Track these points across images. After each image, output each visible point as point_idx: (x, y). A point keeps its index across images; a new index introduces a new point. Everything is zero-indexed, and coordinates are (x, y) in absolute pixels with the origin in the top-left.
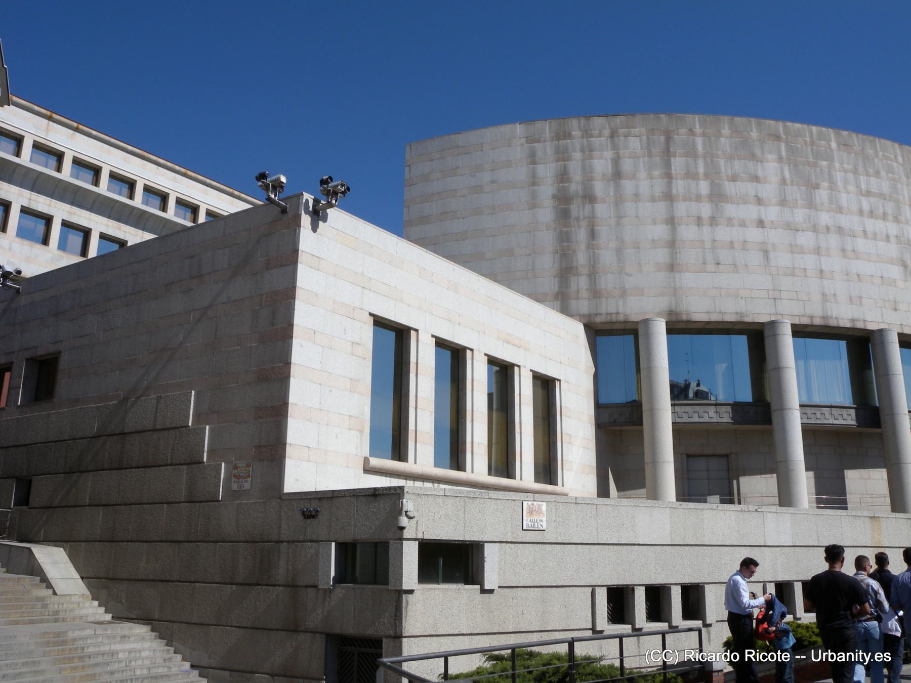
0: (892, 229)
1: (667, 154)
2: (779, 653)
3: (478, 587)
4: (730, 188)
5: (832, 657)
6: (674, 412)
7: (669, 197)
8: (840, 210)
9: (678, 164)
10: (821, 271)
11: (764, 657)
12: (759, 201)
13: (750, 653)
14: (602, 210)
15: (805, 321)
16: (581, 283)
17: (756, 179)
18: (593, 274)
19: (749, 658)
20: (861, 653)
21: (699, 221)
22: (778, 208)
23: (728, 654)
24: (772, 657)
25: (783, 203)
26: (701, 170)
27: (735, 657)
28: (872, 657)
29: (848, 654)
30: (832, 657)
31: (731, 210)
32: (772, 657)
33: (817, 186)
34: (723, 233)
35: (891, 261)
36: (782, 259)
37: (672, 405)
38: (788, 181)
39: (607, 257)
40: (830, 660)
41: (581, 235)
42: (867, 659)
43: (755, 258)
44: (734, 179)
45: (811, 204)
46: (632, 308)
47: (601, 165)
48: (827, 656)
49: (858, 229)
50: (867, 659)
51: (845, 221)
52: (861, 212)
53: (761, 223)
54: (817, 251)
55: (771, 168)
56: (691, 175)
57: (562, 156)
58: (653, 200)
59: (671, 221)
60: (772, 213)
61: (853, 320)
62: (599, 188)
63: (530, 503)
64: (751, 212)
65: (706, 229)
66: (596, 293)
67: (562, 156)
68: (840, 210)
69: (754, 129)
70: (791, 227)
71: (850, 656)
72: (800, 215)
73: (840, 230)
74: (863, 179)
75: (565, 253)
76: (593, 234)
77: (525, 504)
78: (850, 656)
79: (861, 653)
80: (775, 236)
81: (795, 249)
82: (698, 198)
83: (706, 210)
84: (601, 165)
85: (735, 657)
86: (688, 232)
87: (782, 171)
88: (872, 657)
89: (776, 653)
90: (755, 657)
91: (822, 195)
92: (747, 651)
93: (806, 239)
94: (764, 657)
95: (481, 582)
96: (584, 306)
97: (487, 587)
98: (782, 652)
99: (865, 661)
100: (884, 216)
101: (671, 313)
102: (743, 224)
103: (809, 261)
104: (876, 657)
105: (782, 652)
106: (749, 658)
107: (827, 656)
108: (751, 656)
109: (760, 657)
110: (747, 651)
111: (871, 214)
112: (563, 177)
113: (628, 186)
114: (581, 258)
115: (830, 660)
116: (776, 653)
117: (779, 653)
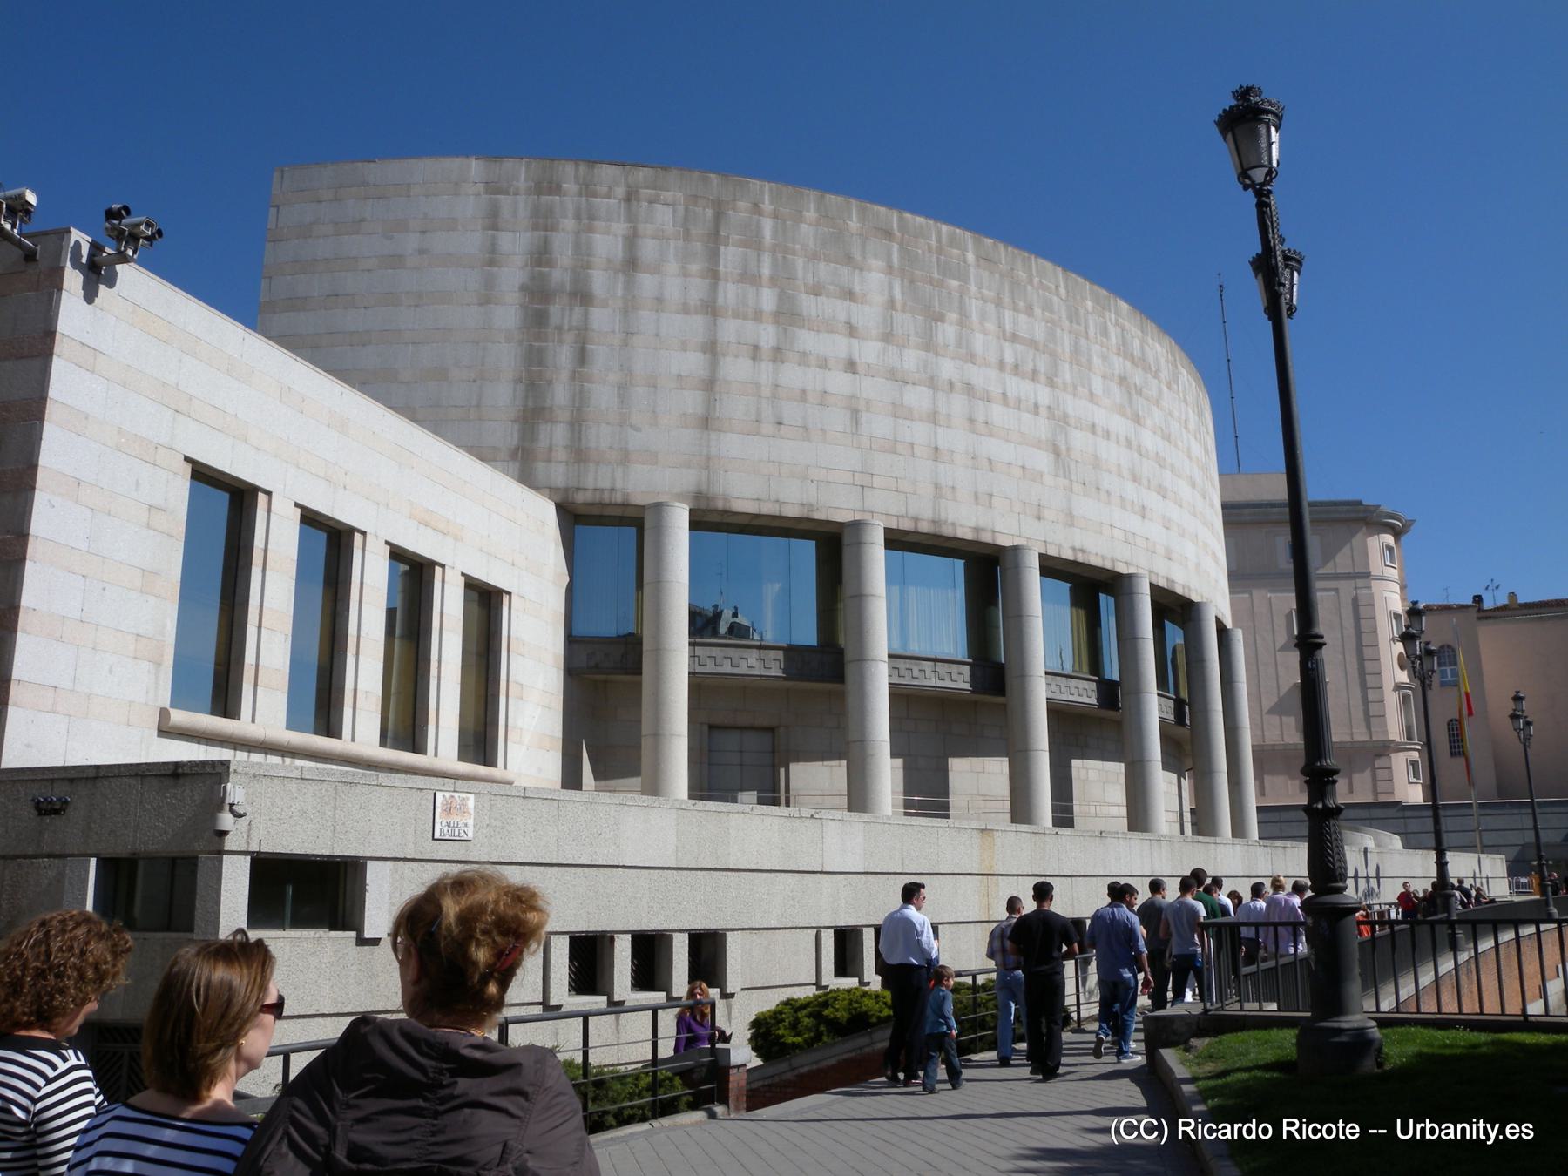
0: (1044, 395)
1: (715, 239)
2: (1341, 1125)
3: (353, 934)
4: (808, 305)
5: (1432, 1131)
6: (692, 656)
7: (711, 309)
8: (971, 358)
9: (730, 256)
10: (937, 449)
11: (1315, 1131)
12: (852, 331)
13: (1291, 1124)
14: (601, 318)
15: (906, 525)
16: (556, 435)
17: (849, 295)
18: (577, 423)
19: (1184, 1132)
20: (1481, 1125)
21: (755, 352)
22: (879, 345)
23: (1253, 1126)
24: (1329, 1131)
25: (887, 337)
26: (766, 272)
27: (1265, 1131)
28: (1501, 1131)
29: (1236, 1126)
30: (1432, 1131)
31: (806, 340)
32: (1329, 1131)
33: (940, 318)
34: (792, 376)
35: (1038, 445)
36: (879, 425)
37: (690, 644)
38: (899, 305)
39: (603, 396)
40: (1428, 1136)
41: (563, 356)
42: (1493, 1135)
43: (837, 420)
44: (816, 291)
45: (929, 345)
46: (637, 484)
47: (607, 244)
48: (1423, 1130)
49: (995, 390)
50: (1493, 1135)
51: (981, 376)
52: (1001, 365)
53: (851, 366)
54: (933, 418)
55: (874, 281)
56: (749, 277)
57: (543, 221)
58: (685, 310)
59: (712, 349)
60: (869, 352)
61: (977, 530)
62: (599, 281)
63: (447, 795)
64: (839, 346)
65: (766, 367)
66: (579, 454)
67: (543, 221)
68: (971, 358)
69: (854, 216)
70: (897, 377)
71: (1463, 1129)
72: (911, 359)
73: (969, 389)
74: (1008, 314)
75: (533, 383)
76: (582, 357)
77: (439, 795)
78: (1463, 1129)
79: (1481, 1125)
80: (872, 389)
81: (899, 411)
82: (758, 316)
83: (767, 335)
84: (607, 244)
85: (1265, 1131)
86: (736, 369)
87: (891, 288)
88: (1501, 1131)
89: (1336, 1123)
90: (1299, 1131)
91: (947, 332)
92: (1285, 1121)
93: (918, 398)
94: (1315, 1131)
95: (359, 929)
96: (559, 474)
97: (367, 935)
98: (1346, 1122)
99: (1488, 1138)
100: (1034, 375)
101: (698, 496)
102: (824, 364)
103: (919, 433)
104: (1508, 1131)
105: (1346, 1122)
106: (1289, 1132)
107: (1423, 1130)
108: (1293, 1129)
109: (1308, 1132)
110: (1285, 1121)
111: (1016, 369)
112: (541, 256)
113: (647, 283)
114: (560, 394)
115: (1428, 1136)
116: (1336, 1123)
117: (1341, 1125)
